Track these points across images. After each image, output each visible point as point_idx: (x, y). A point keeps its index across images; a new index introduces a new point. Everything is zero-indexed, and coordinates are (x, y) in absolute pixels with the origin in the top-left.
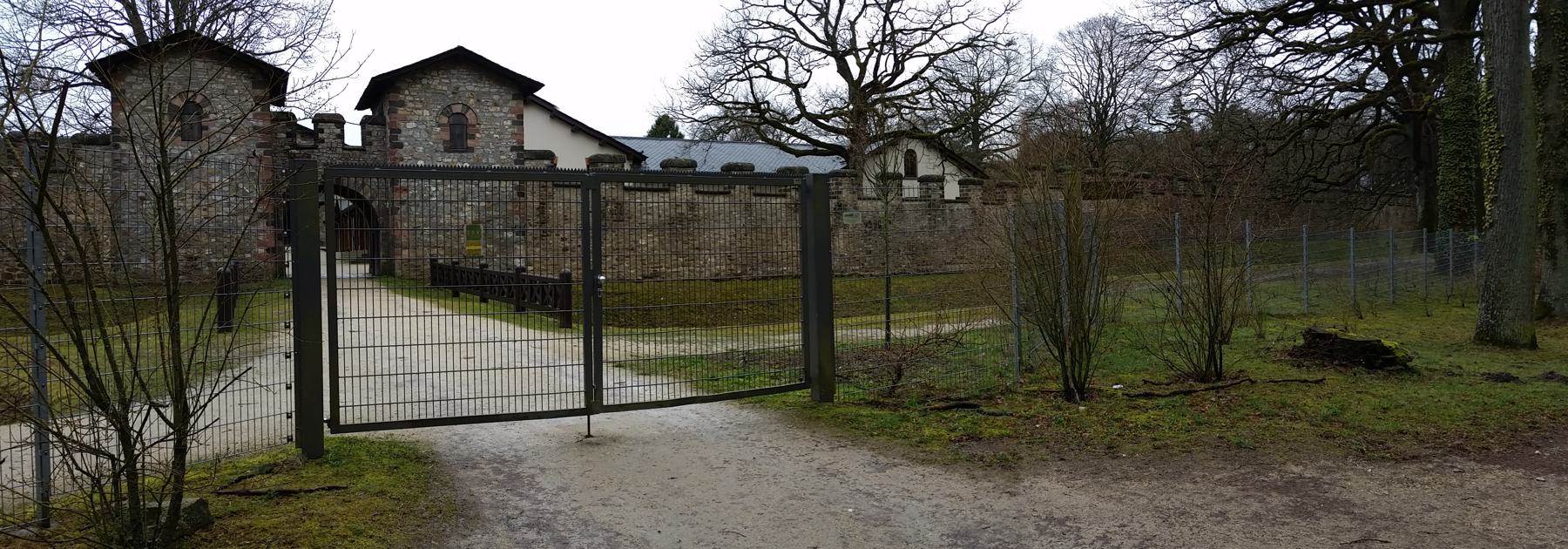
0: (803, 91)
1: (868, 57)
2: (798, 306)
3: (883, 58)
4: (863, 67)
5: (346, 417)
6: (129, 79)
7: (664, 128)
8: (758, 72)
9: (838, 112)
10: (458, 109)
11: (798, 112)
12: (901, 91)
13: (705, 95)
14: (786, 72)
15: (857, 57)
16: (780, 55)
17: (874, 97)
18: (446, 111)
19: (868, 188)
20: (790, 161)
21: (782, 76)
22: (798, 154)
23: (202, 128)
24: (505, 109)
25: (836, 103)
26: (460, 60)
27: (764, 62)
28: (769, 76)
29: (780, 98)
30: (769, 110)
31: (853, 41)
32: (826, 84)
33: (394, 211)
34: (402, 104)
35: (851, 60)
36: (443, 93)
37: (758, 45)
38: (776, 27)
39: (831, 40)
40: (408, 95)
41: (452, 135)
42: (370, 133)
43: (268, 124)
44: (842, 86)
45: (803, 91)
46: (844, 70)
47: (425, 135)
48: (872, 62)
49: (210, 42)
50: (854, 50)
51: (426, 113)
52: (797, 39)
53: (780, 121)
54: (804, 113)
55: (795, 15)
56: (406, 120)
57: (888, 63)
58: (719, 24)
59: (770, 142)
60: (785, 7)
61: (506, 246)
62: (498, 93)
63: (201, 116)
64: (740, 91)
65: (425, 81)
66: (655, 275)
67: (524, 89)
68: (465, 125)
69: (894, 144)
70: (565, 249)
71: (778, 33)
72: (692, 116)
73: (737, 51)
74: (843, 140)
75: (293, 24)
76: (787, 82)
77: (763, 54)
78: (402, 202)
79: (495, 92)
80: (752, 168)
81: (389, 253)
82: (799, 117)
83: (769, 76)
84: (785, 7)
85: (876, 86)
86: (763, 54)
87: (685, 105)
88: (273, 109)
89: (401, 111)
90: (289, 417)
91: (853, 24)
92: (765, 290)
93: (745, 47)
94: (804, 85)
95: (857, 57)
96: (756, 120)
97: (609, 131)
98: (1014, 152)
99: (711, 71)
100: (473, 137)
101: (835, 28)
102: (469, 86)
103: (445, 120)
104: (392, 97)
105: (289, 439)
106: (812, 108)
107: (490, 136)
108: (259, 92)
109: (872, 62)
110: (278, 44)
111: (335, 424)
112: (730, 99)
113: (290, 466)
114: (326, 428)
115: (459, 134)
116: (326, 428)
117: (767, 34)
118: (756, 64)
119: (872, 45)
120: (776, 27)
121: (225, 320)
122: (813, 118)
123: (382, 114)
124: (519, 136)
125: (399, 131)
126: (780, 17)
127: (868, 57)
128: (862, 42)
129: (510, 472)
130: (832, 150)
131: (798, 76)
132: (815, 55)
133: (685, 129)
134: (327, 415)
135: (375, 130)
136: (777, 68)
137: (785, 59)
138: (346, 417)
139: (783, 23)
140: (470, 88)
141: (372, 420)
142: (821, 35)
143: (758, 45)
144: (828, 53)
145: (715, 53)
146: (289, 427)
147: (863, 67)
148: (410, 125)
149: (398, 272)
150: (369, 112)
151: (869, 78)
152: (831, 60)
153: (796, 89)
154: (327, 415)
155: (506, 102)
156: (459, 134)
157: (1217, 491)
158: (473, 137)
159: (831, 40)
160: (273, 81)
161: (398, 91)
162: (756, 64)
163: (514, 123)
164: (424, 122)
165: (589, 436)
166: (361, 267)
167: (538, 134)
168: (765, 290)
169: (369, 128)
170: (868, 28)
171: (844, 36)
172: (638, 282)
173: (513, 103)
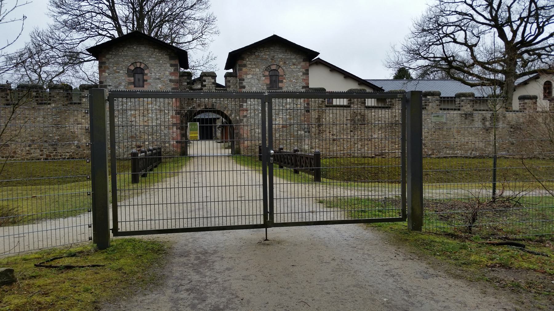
0: (475, 49)
1: (519, 26)
2: (86, 167)
3: (529, 25)
4: (515, 32)
5: (122, 227)
6: (107, 56)
7: (402, 74)
8: (448, 39)
9: (497, 61)
10: (274, 67)
11: (472, 61)
12: (538, 46)
13: (416, 54)
14: (466, 38)
15: (511, 26)
16: (462, 29)
17: (524, 49)
18: (268, 69)
19: (516, 104)
20: (467, 89)
21: (463, 41)
22: (472, 85)
23: (144, 81)
24: (299, 67)
25: (499, 55)
26: (275, 42)
27: (451, 34)
28: (455, 41)
29: (463, 53)
30: (454, 61)
31: (510, 17)
32: (490, 42)
33: (241, 121)
34: (245, 66)
35: (507, 29)
36: (266, 59)
37: (447, 25)
38: (460, 13)
39: (495, 19)
40: (248, 61)
41: (271, 81)
42: (229, 81)
43: (177, 78)
44: (500, 43)
45: (475, 49)
46: (502, 35)
47: (257, 81)
48: (521, 29)
49: (148, 37)
50: (509, 22)
51: (257, 70)
52: (473, 19)
53: (463, 67)
54: (476, 62)
55: (471, 6)
56: (246, 74)
57: (532, 29)
58: (425, 14)
59: (455, 79)
60: (465, 2)
61: (299, 139)
62: (295, 58)
63: (143, 74)
64: (437, 51)
65: (257, 54)
66: (382, 154)
67: (309, 56)
68: (277, 76)
69: (536, 78)
70: (334, 140)
71: (460, 17)
72: (415, 67)
73: (434, 27)
74: (500, 77)
75: (196, 27)
76: (466, 44)
77: (450, 29)
78: (245, 116)
79: (294, 58)
80: (325, 90)
81: (239, 143)
82: (473, 65)
83: (455, 41)
84: (465, 2)
85: (524, 43)
86: (450, 29)
87: (405, 60)
88: (182, 69)
89: (244, 69)
90: (90, 227)
91: (509, 8)
92: (444, 164)
93: (440, 26)
94: (476, 45)
95: (511, 26)
96: (451, 67)
97: (363, 76)
98: (444, 73)
99: (420, 40)
100: (282, 82)
101: (497, 11)
102: (280, 55)
103: (267, 73)
104: (239, 62)
105: (90, 239)
106: (481, 58)
107: (291, 81)
108: (173, 62)
109: (521, 29)
110: (189, 37)
111: (116, 232)
112: (432, 55)
113: (89, 253)
114: (111, 234)
115: (274, 78)
116: (111, 234)
117: (453, 18)
118: (447, 35)
119: (521, 19)
120: (460, 13)
121: (135, 180)
122: (482, 64)
123: (236, 71)
124: (307, 80)
125: (244, 80)
126: (463, 8)
127: (519, 26)
128: (515, 17)
129: (204, 259)
130: (493, 83)
131: (472, 41)
132: (483, 28)
133: (413, 74)
134: (111, 227)
135: (232, 79)
136: (460, 36)
137: (465, 31)
138: (122, 227)
139: (464, 11)
140: (280, 56)
141: (128, 230)
142: (488, 16)
143: (447, 25)
144: (493, 26)
145: (423, 30)
146: (90, 232)
147: (515, 32)
148: (249, 76)
149: (242, 152)
150: (231, 71)
151: (519, 38)
152: (495, 30)
153: (471, 47)
154: (111, 227)
155: (299, 63)
156: (274, 78)
157: (96, 298)
158: (282, 82)
159: (495, 19)
160: (180, 57)
161: (243, 59)
162: (447, 35)
163: (304, 74)
164: (256, 74)
165: (266, 240)
166: (227, 150)
167: (318, 79)
168: (444, 164)
169: (229, 78)
170: (519, 9)
171: (503, 15)
172: (373, 157)
173: (303, 64)
